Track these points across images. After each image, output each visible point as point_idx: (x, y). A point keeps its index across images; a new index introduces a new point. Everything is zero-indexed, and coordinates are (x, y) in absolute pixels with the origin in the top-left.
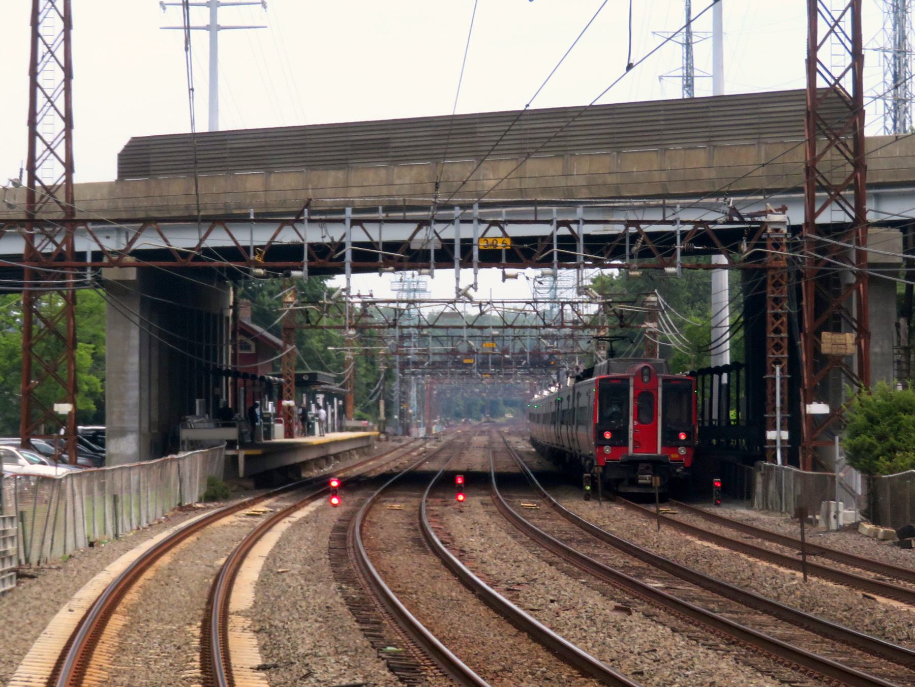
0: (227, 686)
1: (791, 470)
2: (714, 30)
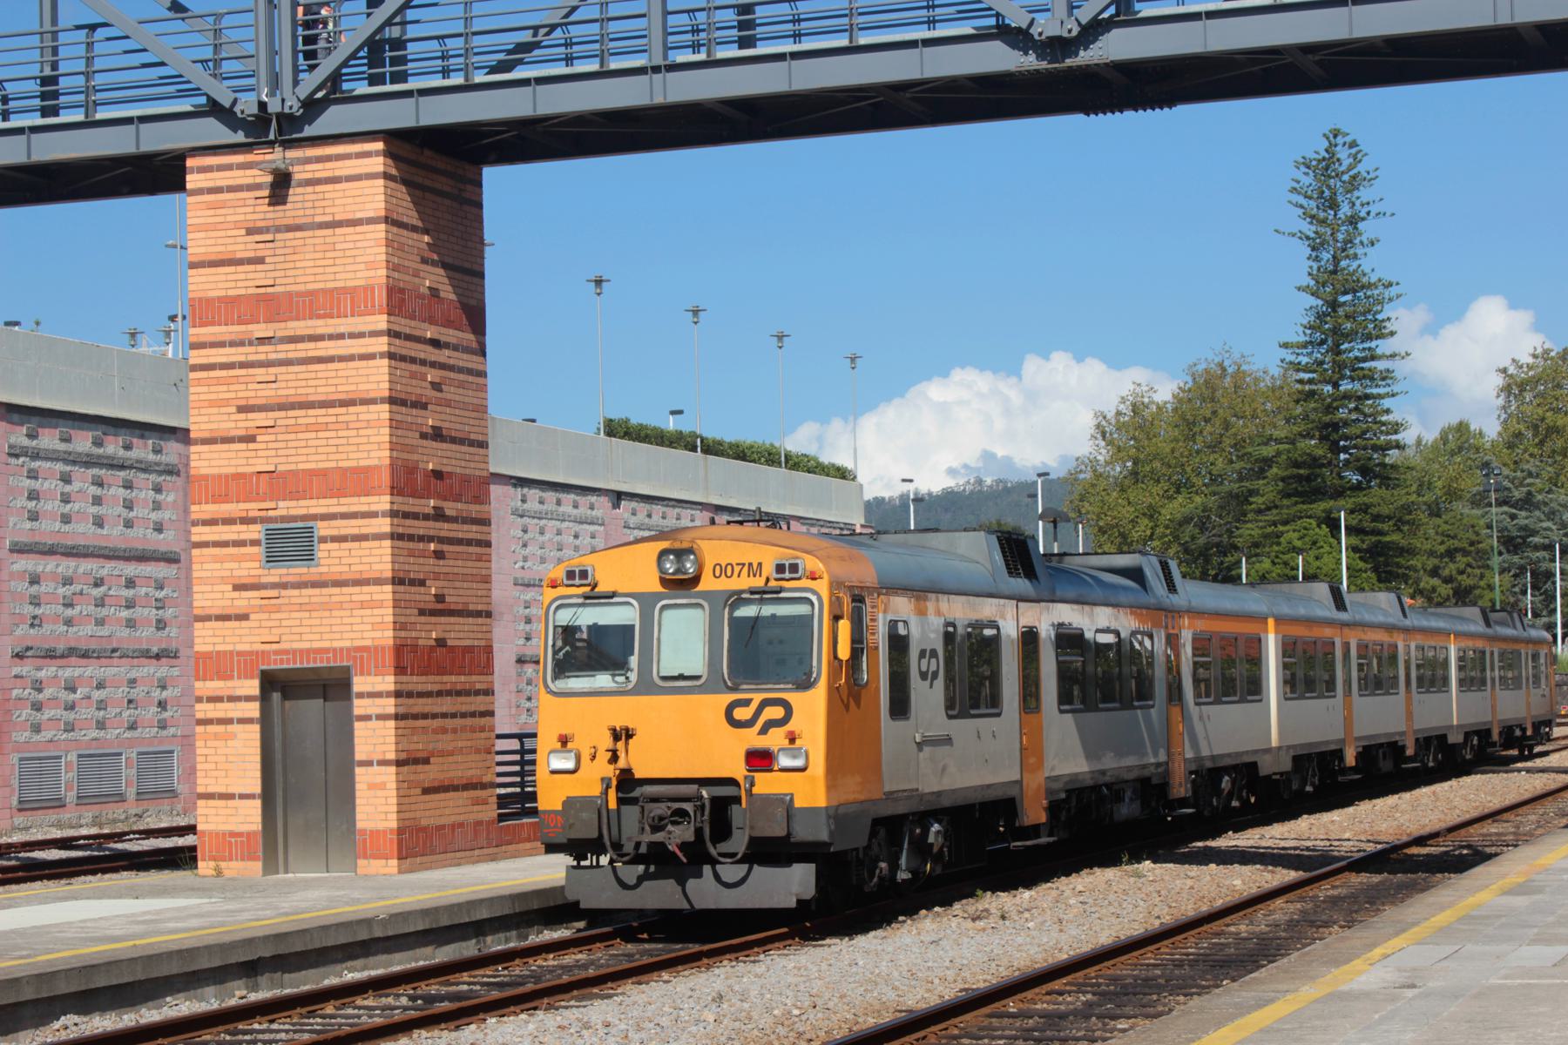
0: (1564, 753)
1: (523, 824)
2: (482, 251)
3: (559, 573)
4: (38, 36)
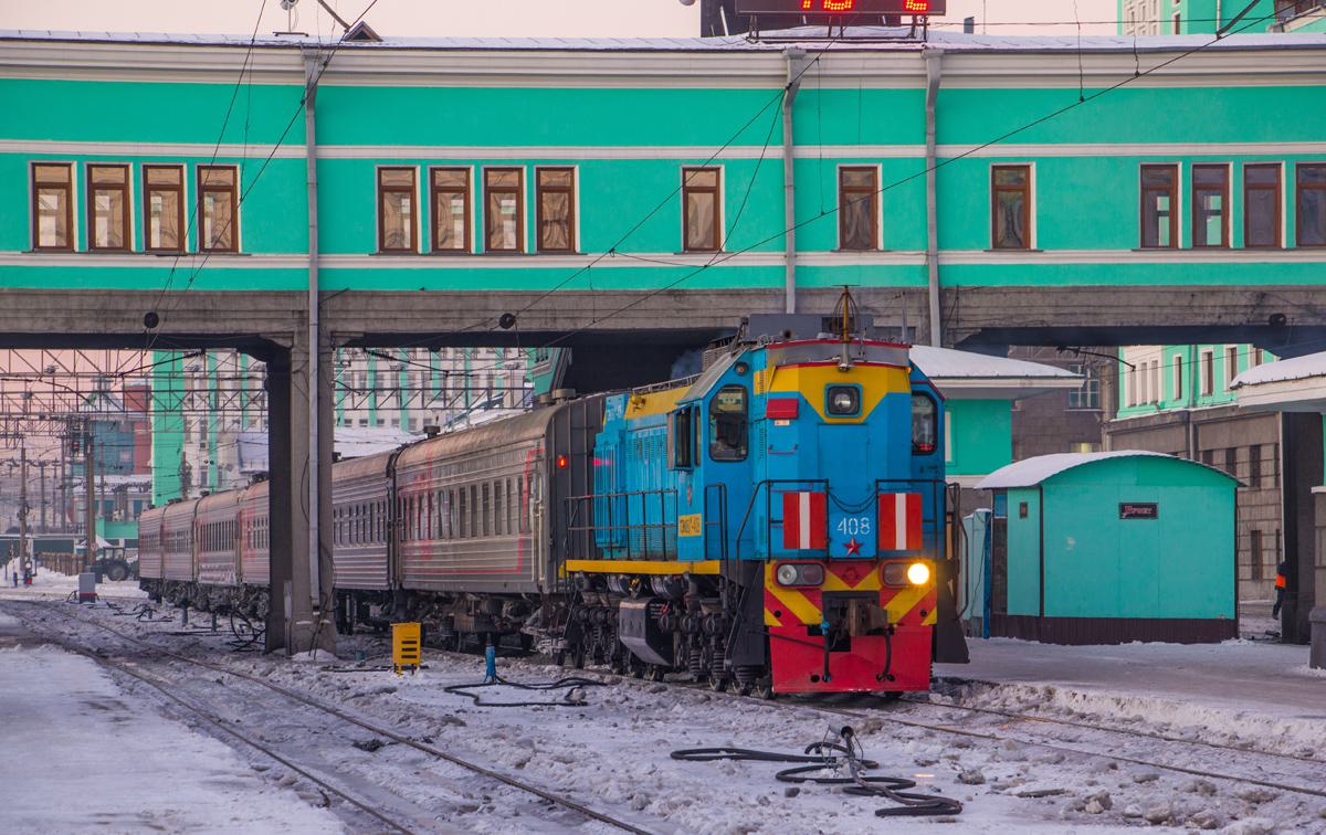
0: (1324, 170)
2: (105, 348)
3: (25, 446)
4: (932, 518)
